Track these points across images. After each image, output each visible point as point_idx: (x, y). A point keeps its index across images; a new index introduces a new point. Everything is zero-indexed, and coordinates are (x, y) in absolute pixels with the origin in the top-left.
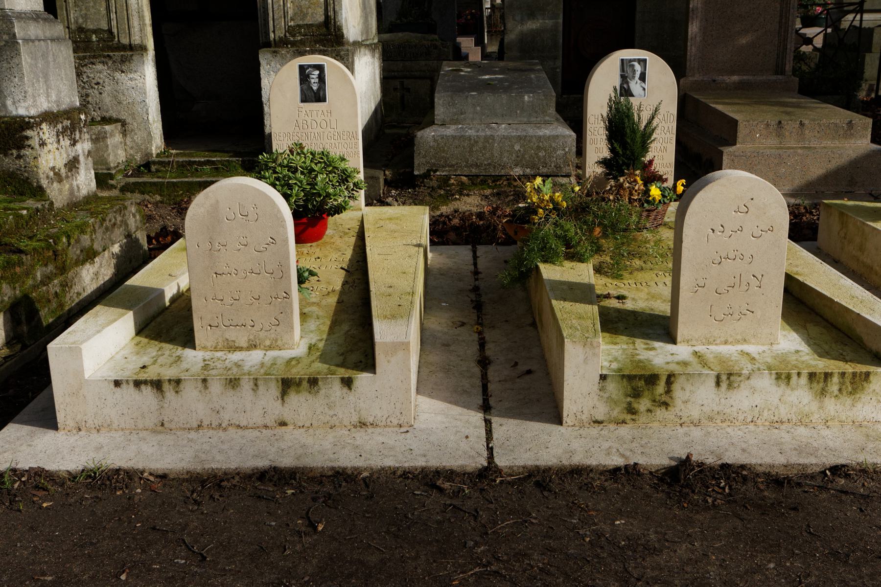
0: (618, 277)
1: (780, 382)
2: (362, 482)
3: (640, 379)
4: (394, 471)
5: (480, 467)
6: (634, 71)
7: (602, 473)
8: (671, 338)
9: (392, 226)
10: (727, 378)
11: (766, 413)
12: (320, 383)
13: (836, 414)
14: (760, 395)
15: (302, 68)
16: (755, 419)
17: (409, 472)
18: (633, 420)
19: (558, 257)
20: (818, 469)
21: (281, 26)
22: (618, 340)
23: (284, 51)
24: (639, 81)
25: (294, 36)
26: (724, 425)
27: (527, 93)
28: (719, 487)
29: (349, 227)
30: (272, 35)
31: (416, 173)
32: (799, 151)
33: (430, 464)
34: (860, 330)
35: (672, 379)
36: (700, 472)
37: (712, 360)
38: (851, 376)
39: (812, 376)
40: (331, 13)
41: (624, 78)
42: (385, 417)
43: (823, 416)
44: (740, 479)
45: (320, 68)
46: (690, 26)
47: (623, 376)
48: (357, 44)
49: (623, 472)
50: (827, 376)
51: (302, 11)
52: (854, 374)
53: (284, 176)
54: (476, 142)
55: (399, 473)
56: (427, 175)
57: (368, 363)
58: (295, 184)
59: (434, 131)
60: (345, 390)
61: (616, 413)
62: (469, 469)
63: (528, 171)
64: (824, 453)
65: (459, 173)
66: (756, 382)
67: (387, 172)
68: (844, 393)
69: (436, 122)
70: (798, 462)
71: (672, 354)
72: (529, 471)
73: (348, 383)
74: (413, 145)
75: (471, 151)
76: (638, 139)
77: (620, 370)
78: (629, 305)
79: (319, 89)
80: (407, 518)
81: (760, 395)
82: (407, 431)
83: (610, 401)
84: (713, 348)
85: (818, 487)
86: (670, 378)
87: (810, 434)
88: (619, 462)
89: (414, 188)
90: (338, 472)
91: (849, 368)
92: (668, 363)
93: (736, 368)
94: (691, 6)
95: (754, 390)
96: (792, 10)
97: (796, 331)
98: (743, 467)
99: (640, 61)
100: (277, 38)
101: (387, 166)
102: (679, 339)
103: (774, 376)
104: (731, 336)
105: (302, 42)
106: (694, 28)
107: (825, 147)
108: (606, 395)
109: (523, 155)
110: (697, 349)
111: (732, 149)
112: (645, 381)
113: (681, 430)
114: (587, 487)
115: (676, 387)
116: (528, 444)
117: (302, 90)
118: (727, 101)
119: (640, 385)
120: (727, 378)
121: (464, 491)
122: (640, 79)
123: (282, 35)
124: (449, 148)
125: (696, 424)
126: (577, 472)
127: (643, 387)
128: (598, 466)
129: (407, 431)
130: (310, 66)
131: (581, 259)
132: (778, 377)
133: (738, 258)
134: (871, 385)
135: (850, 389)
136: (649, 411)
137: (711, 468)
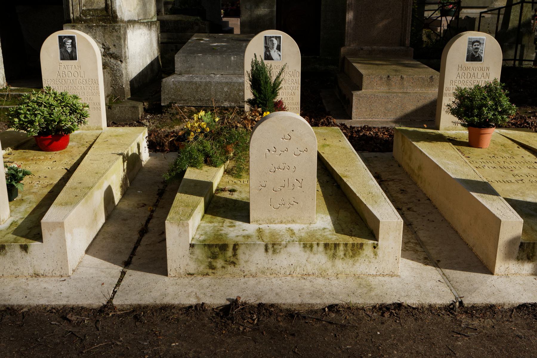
0: (239, 176)
1: (306, 249)
2: (21, 315)
3: (216, 247)
4: (45, 308)
5: (102, 305)
6: (273, 44)
7: (181, 309)
8: (247, 219)
9: (114, 141)
10: (272, 246)
11: (298, 269)
12: (6, 248)
13: (343, 270)
14: (293, 258)
15: (61, 38)
17: (54, 309)
18: (213, 273)
19: (200, 163)
20: (321, 307)
21: (77, 10)
22: (214, 220)
24: (276, 51)
25: (86, 16)
26: (272, 276)
27: (234, 55)
28: (252, 319)
29: (87, 140)
30: (72, 15)
31: (163, 104)
32: (400, 95)
33: (69, 303)
34: (366, 215)
35: (237, 247)
36: (242, 309)
37: (267, 234)
39: (326, 246)
41: (267, 48)
42: (51, 271)
43: (335, 271)
44: (268, 314)
45: (279, 38)
46: (347, 15)
47: (205, 245)
48: (132, 22)
50: (336, 245)
52: (353, 245)
53: (33, 109)
54: (200, 86)
55: (48, 309)
56: (169, 106)
57: (38, 237)
58: (39, 114)
60: (24, 253)
61: (202, 268)
62: (95, 306)
63: (233, 104)
64: (327, 296)
65: (189, 105)
67: (145, 104)
68: (348, 256)
69: (176, 72)
70: (309, 302)
71: (243, 230)
72: (134, 307)
73: (25, 248)
75: (197, 91)
76: (270, 90)
77: (204, 240)
78: (235, 196)
79: (72, 52)
80: (37, 341)
81: (293, 258)
82: (65, 280)
83: (197, 260)
84: (272, 226)
85: (317, 319)
86: (236, 247)
87: (324, 283)
88: (193, 301)
89: (162, 114)
90: (8, 308)
91: (350, 240)
92: (238, 236)
93: (280, 240)
95: (290, 255)
96: (409, 7)
97: (331, 214)
98: (272, 305)
100: (75, 17)
101: (146, 100)
102: (251, 220)
103: (302, 246)
104: (285, 218)
105: (91, 20)
106: (350, 16)
107: (416, 93)
108: (195, 257)
109: (230, 94)
110: (261, 226)
111: (359, 92)
112: (220, 248)
113: (243, 280)
114: (166, 319)
115: (240, 252)
116: (145, 289)
117: (61, 52)
119: (216, 251)
120: (272, 246)
121: (84, 322)
122: (277, 49)
123: (78, 15)
124: (183, 89)
126: (165, 308)
127: (218, 252)
129: (65, 280)
130: (65, 37)
131: (214, 165)
132: (305, 246)
133: (286, 169)
134: (364, 252)
135: (351, 254)
136: (223, 267)
137: (252, 307)
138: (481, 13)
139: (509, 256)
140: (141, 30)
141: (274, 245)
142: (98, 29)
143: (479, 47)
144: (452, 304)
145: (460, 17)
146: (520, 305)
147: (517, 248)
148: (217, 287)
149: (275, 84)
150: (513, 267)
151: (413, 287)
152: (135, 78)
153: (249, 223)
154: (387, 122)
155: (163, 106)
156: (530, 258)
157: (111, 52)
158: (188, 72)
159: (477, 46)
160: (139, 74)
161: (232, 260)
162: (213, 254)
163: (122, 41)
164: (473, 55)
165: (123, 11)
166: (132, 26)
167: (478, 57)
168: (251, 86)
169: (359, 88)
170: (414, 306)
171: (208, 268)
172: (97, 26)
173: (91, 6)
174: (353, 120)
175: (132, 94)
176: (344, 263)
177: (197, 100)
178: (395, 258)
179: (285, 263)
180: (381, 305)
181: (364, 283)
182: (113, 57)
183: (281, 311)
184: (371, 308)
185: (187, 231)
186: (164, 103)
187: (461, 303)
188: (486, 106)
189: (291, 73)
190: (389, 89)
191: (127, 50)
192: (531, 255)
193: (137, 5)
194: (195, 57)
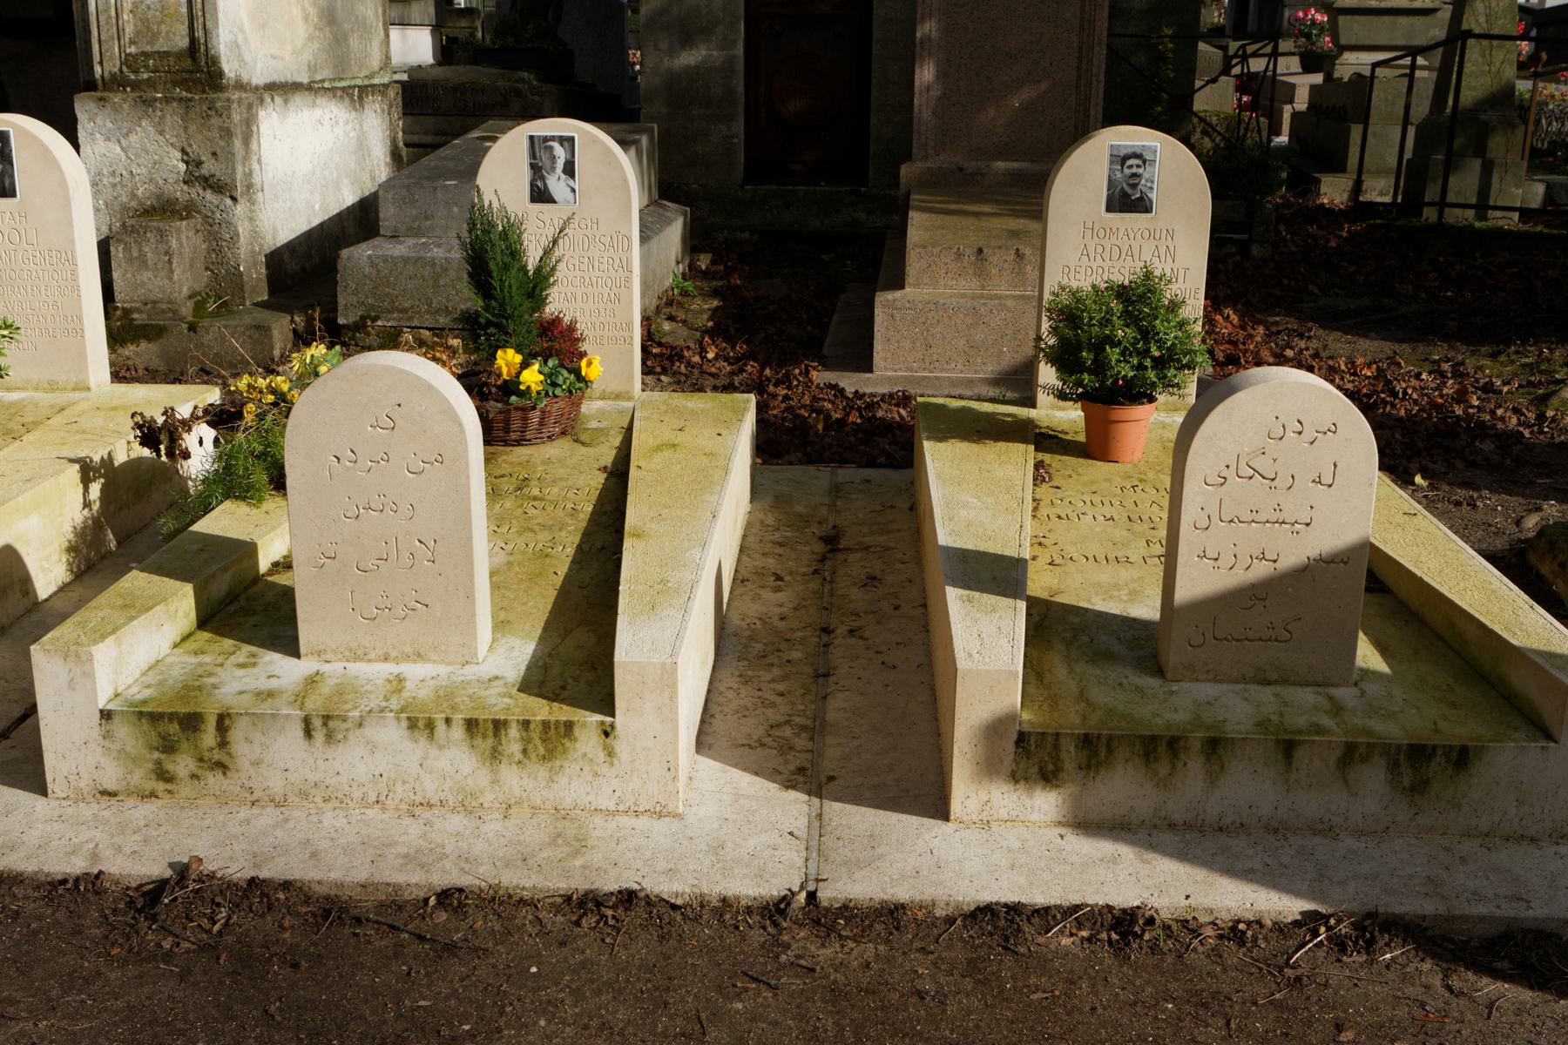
6: (554, 158)
8: (289, 645)
10: (323, 724)
11: (399, 788)
13: (524, 795)
14: (379, 756)
16: (382, 798)
18: (169, 792)
23: (117, 99)
24: (563, 177)
25: (136, 72)
30: (98, 70)
31: (341, 321)
32: (1010, 303)
35: (227, 722)
36: (197, 891)
38: (540, 727)
39: (471, 725)
40: (199, 34)
41: (537, 170)
48: (283, 89)
49: (69, 886)
50: (499, 726)
51: (148, 28)
52: (546, 725)
59: (374, 248)
61: (140, 777)
65: (416, 323)
66: (373, 731)
67: (297, 318)
68: (533, 756)
74: (336, 271)
75: (436, 286)
77: (144, 702)
81: (379, 756)
83: (122, 755)
86: (223, 722)
88: (77, 866)
94: (918, 35)
96: (1097, 48)
98: (286, 885)
99: (562, 140)
102: (303, 650)
103: (404, 723)
105: (151, 84)
106: (925, 74)
112: (180, 724)
113: (244, 813)
118: (954, 207)
123: (116, 70)
124: (396, 278)
125: (280, 803)
128: (36, 873)
132: (412, 724)
134: (578, 745)
135: (542, 751)
136: (194, 776)
137: (231, 885)
138: (1375, 65)
139: (989, 768)
140: (318, 112)
141: (327, 718)
142: (169, 109)
143: (1141, 171)
144: (784, 898)
145: (1336, 75)
146: (978, 909)
147: (1011, 748)
148: (163, 829)
149: (538, 270)
150: (1004, 799)
151: (703, 846)
152: (290, 246)
153: (298, 657)
154: (971, 381)
155: (343, 326)
156: (1048, 777)
157: (205, 171)
158: (416, 232)
159: (1134, 170)
160: (308, 235)
161: (216, 757)
162: (163, 738)
163: (237, 144)
164: (1125, 195)
165: (247, 58)
166: (277, 99)
167: (1141, 199)
168: (470, 275)
169: (899, 284)
170: (679, 902)
171: (153, 776)
172: (167, 100)
173: (151, 43)
174: (878, 373)
175: (272, 291)
176: (525, 777)
177: (438, 311)
178: (666, 766)
179: (362, 771)
180: (587, 893)
181: (571, 832)
182: (211, 187)
183: (308, 899)
184: (559, 900)
185: (90, 675)
186: (346, 317)
187: (812, 896)
188: (1115, 344)
189: (607, 241)
190: (983, 288)
191: (256, 167)
192: (1051, 767)
193: (310, 39)
194: (435, 189)
